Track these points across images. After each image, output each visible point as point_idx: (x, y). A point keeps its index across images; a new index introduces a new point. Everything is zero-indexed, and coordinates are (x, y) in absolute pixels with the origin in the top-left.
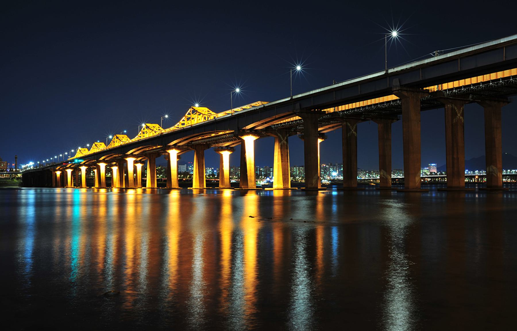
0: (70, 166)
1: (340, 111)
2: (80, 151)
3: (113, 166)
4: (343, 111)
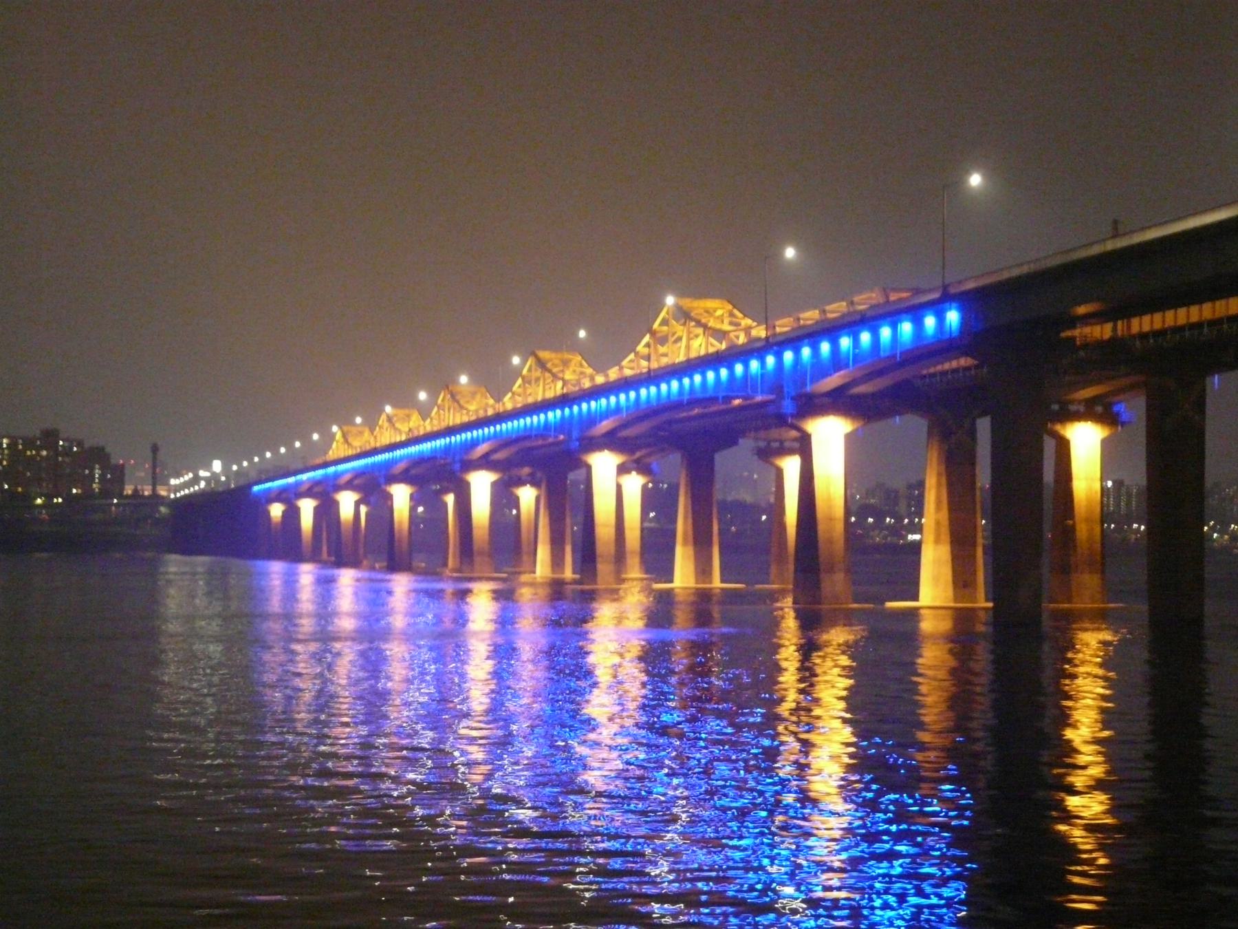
0: (486, 456)
1: (1133, 337)
2: (390, 419)
3: (520, 482)
4: (1143, 336)
